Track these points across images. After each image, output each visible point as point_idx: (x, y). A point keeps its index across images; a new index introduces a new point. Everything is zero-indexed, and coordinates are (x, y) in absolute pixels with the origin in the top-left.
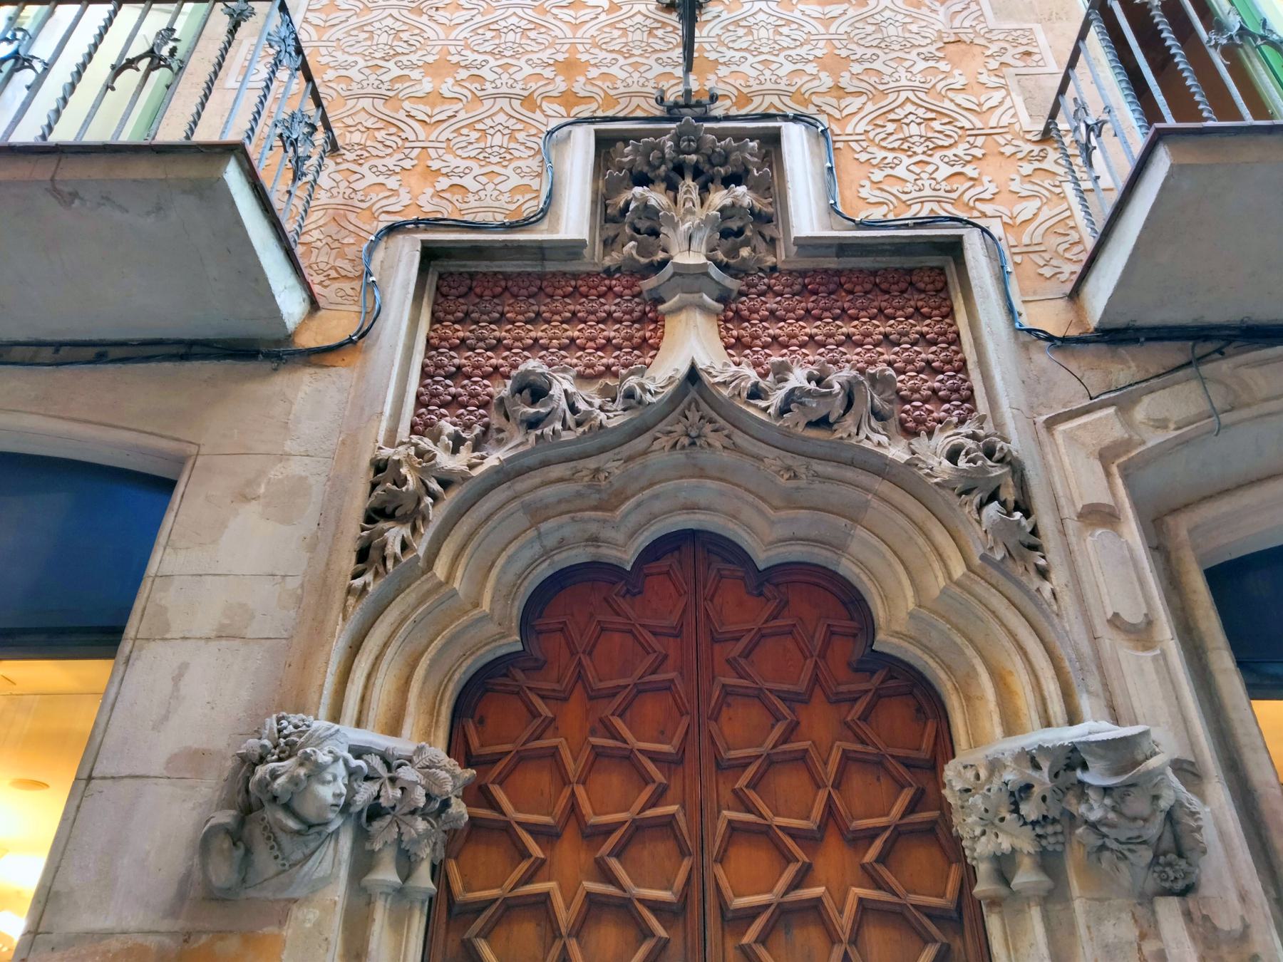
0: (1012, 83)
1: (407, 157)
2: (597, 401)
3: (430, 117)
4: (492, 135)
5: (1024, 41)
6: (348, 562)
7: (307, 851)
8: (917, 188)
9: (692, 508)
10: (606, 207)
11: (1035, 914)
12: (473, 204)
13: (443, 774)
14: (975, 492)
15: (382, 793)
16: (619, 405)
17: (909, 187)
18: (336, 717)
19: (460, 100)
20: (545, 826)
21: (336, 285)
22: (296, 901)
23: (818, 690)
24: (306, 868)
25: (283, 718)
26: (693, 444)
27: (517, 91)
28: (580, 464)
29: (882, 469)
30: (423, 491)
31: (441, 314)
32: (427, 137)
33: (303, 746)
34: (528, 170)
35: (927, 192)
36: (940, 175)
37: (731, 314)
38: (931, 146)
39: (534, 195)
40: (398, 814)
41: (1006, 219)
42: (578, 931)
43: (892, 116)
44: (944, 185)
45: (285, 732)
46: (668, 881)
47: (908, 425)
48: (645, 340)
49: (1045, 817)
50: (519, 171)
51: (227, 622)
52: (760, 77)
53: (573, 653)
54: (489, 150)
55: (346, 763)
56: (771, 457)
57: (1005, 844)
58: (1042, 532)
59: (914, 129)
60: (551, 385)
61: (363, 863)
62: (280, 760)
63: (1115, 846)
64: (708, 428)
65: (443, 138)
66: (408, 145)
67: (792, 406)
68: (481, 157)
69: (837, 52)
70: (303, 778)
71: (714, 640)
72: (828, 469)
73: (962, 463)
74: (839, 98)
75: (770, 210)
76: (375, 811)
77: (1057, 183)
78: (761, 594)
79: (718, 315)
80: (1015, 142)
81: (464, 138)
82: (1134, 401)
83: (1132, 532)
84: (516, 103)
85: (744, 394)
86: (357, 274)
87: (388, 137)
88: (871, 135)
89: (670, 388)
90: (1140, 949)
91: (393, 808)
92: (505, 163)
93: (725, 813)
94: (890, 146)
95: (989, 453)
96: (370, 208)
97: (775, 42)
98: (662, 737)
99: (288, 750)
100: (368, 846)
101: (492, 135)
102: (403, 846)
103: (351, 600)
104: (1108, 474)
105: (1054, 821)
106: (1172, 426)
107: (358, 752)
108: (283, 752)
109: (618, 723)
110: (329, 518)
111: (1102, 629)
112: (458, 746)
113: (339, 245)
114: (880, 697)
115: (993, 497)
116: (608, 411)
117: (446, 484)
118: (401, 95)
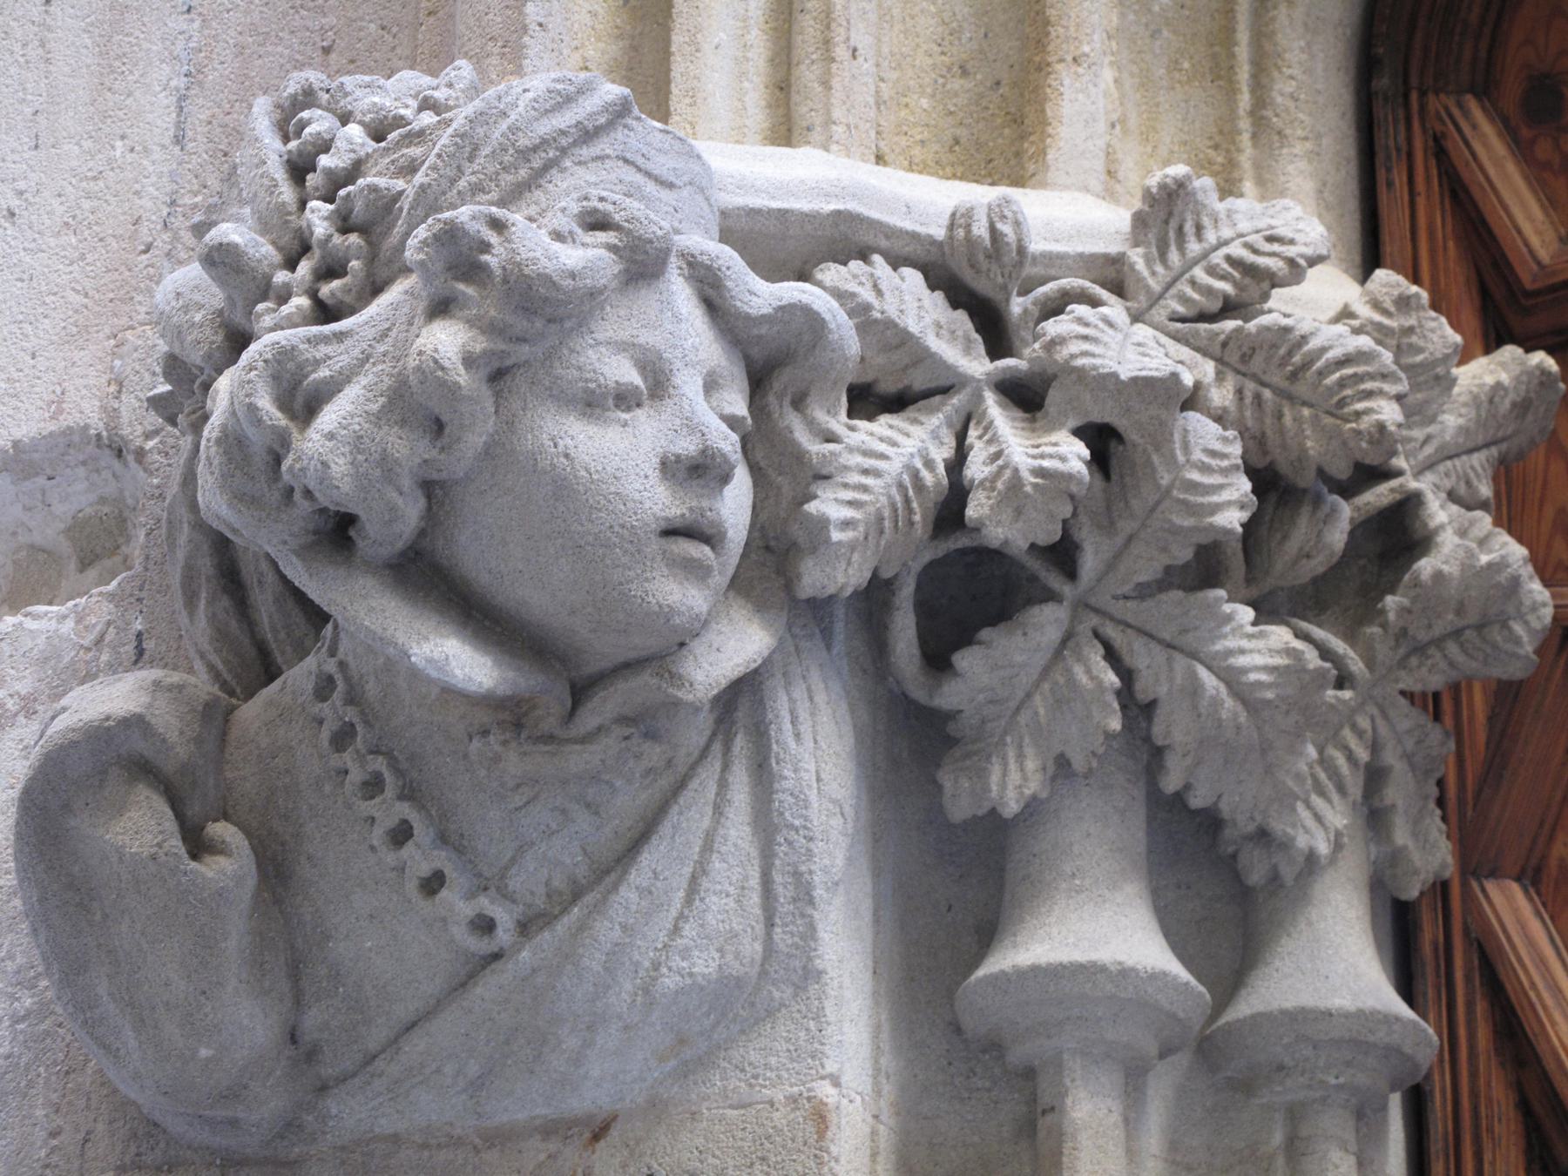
15: (977, 468)
24: (607, 931)
25: (307, 98)
40: (1103, 600)
70: (462, 377)
91: (1063, 554)
100: (960, 804)
102: (1171, 783)
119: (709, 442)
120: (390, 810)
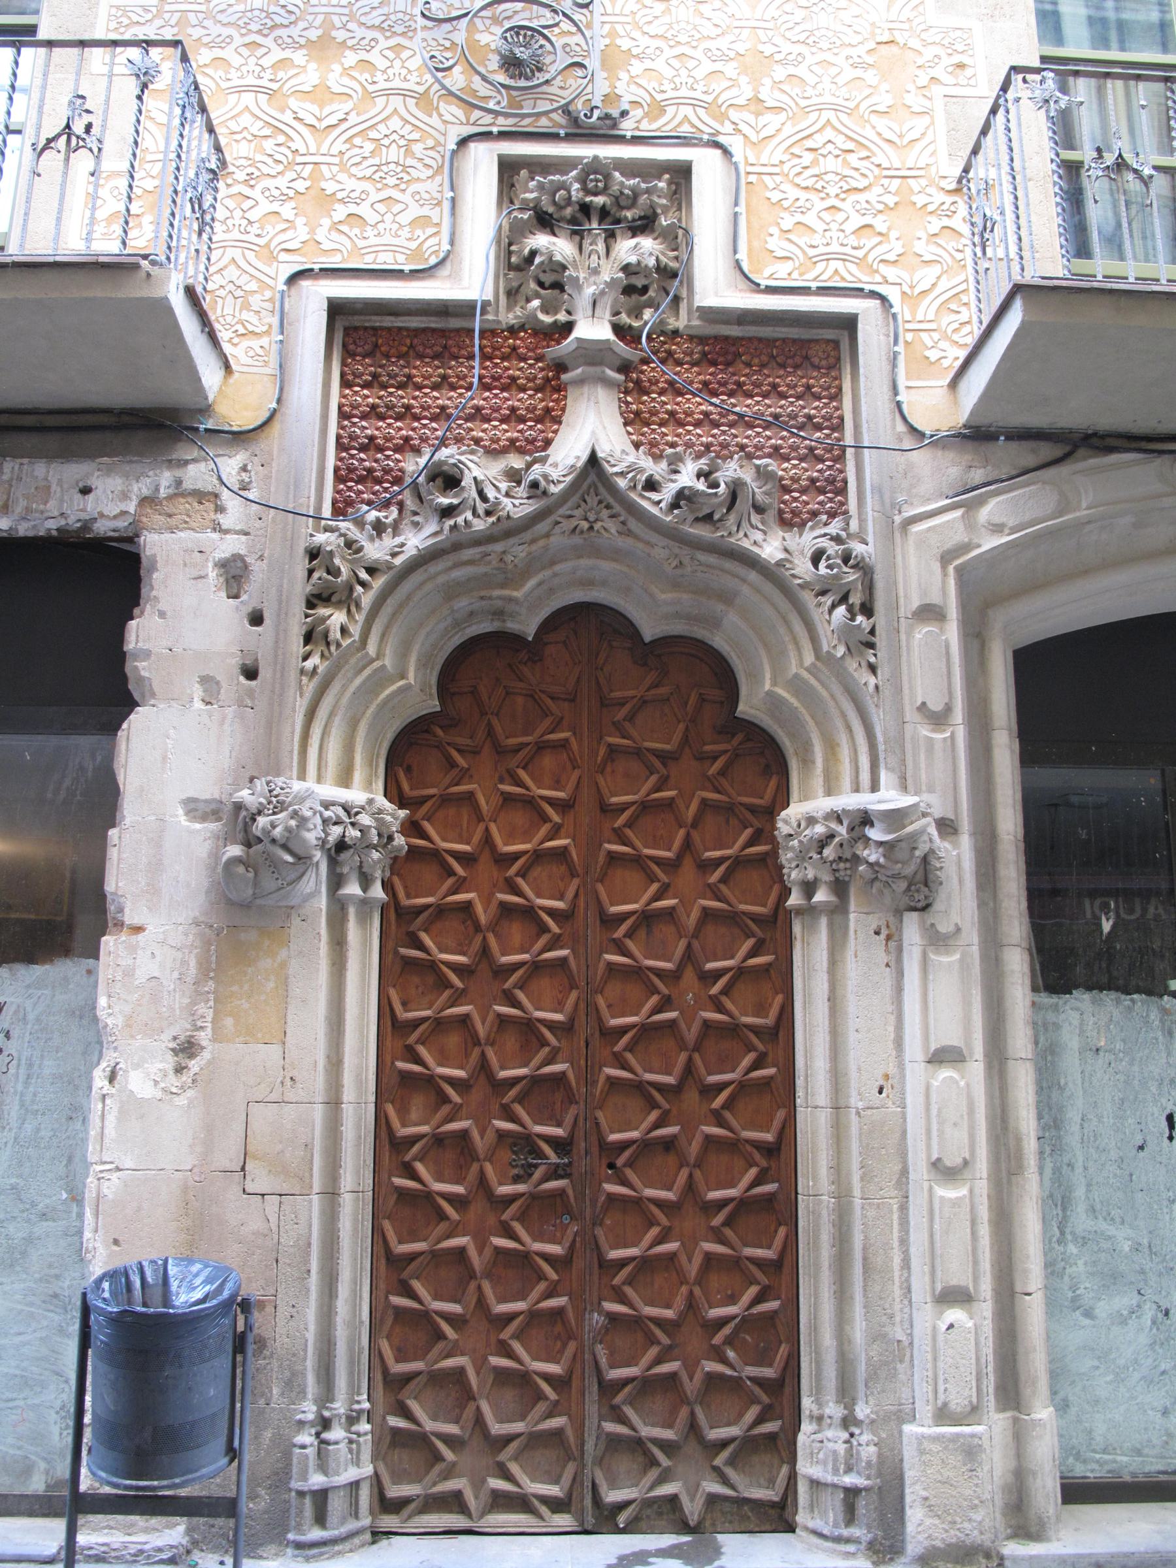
0: (939, 105)
1: (299, 177)
2: (504, 486)
3: (319, 120)
4: (387, 147)
5: (960, 48)
6: (296, 645)
9: (589, 583)
10: (510, 253)
11: (824, 921)
12: (373, 241)
13: (389, 818)
14: (830, 594)
16: (522, 491)
17: (817, 239)
18: (302, 776)
19: (350, 96)
20: (465, 853)
21: (246, 343)
23: (687, 750)
26: (591, 528)
27: (410, 85)
28: (489, 548)
29: (752, 562)
30: (354, 581)
31: (350, 378)
32: (318, 150)
33: (290, 805)
34: (427, 196)
35: (835, 247)
36: (850, 227)
38: (846, 187)
39: (435, 230)
41: (906, 289)
42: (494, 926)
43: (810, 144)
44: (853, 241)
45: (275, 793)
46: (559, 1004)
48: (548, 410)
49: (840, 858)
50: (417, 197)
52: (675, 79)
53: (483, 714)
56: (660, 544)
57: (810, 874)
58: (877, 633)
59: (831, 164)
60: (462, 472)
61: (336, 881)
62: (274, 813)
63: (884, 879)
64: (605, 513)
65: (334, 151)
66: (299, 159)
67: (682, 503)
69: (761, 47)
71: (602, 704)
72: (712, 559)
73: (823, 569)
74: (758, 114)
75: (673, 265)
76: (342, 845)
77: (961, 248)
78: (645, 664)
79: (619, 386)
81: (356, 151)
82: (981, 501)
83: (952, 632)
84: (411, 102)
85: (639, 487)
86: (265, 329)
87: (277, 148)
88: (786, 167)
89: (568, 479)
92: (403, 186)
93: (607, 846)
94: (804, 184)
95: (846, 558)
96: (268, 245)
97: (695, 28)
98: (557, 785)
99: (281, 807)
100: (338, 870)
101: (387, 147)
103: (305, 679)
104: (945, 575)
105: (847, 860)
106: (1007, 531)
107: (327, 805)
108: (275, 807)
109: (522, 773)
111: (910, 714)
112: (394, 792)
113: (242, 294)
114: (737, 755)
115: (844, 599)
116: (513, 497)
117: (371, 571)
118: (285, 88)
119: (144, 519)
120: (272, 869)
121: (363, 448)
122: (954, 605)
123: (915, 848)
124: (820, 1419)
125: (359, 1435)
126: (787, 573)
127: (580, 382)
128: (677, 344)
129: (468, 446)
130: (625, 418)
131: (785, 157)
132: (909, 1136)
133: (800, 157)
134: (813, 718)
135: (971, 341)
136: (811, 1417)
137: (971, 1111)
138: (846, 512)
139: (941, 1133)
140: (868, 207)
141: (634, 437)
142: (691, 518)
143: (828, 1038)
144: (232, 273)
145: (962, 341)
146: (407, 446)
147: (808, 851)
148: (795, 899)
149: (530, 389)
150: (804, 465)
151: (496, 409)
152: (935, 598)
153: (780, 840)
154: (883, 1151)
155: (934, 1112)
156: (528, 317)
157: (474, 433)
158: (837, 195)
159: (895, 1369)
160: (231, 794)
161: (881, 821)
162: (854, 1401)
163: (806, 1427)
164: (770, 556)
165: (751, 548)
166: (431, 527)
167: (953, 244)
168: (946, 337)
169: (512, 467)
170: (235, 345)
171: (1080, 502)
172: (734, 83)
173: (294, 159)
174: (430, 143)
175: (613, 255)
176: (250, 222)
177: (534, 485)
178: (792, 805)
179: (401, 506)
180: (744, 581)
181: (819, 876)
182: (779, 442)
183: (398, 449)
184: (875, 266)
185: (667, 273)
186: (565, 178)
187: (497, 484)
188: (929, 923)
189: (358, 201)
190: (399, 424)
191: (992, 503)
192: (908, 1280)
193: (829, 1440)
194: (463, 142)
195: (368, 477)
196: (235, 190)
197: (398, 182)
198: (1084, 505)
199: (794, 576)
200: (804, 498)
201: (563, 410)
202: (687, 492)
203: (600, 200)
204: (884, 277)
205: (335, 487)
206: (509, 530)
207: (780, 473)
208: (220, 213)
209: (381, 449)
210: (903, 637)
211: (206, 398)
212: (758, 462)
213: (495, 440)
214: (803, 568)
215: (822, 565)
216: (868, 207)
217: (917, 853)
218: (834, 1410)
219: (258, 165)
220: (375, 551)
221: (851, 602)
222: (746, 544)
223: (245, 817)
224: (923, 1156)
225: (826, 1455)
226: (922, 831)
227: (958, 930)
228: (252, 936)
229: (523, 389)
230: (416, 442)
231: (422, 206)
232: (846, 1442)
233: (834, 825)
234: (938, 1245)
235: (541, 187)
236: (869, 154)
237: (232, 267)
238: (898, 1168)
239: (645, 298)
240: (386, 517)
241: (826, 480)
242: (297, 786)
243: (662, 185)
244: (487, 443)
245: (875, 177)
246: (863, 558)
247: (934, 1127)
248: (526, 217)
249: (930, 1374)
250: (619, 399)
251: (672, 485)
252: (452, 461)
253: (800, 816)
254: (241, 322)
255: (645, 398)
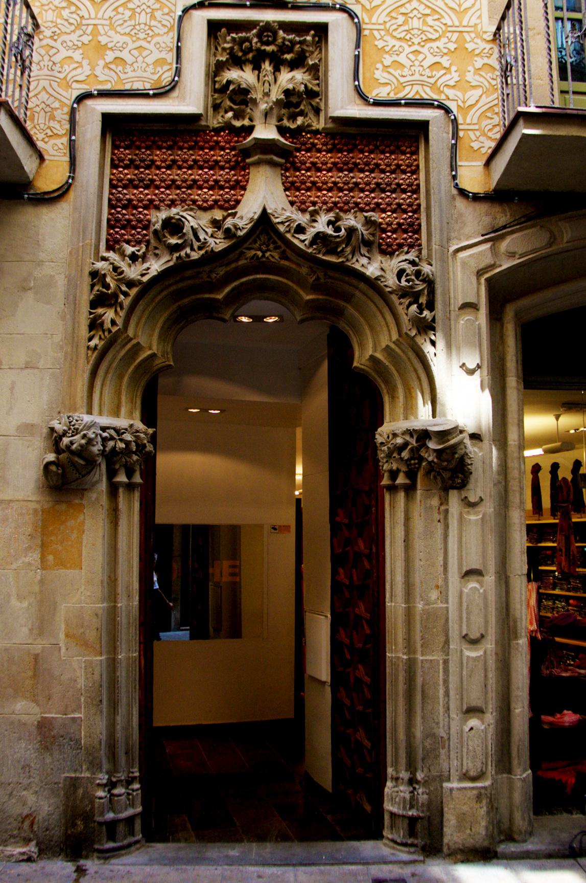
2: (210, 231)
4: (139, 14)
6: (84, 331)
7: (88, 471)
8: (411, 73)
12: (131, 74)
13: (142, 435)
16: (220, 234)
17: (406, 72)
21: (53, 141)
22: (86, 490)
29: (362, 277)
31: (117, 162)
32: (96, 15)
33: (82, 430)
35: (417, 77)
36: (426, 64)
37: (289, 165)
38: (424, 38)
41: (460, 103)
43: (403, 10)
44: (428, 72)
45: (73, 423)
47: (383, 247)
51: (29, 360)
54: (137, 27)
55: (101, 435)
61: (111, 473)
62: (72, 436)
64: (271, 246)
65: (106, 16)
68: (132, 33)
75: (316, 89)
77: (495, 77)
80: (476, 40)
81: (120, 16)
82: (502, 237)
88: (388, 25)
89: (249, 226)
90: (439, 509)
92: (149, 39)
94: (398, 36)
96: (65, 78)
99: (76, 431)
103: (90, 352)
104: (479, 283)
106: (517, 256)
107: (104, 429)
108: (73, 432)
110: (71, 300)
113: (50, 109)
115: (416, 301)
116: (215, 238)
121: (124, 207)
122: (484, 303)
123: (456, 453)
124: (397, 779)
125: (133, 790)
126: (382, 284)
127: (258, 163)
128: (318, 139)
129: (189, 205)
130: (285, 186)
131: (387, 19)
132: (450, 621)
133: (396, 19)
134: (398, 371)
135: (498, 136)
136: (392, 778)
137: (486, 606)
138: (420, 245)
139: (468, 619)
140: (438, 51)
141: (290, 198)
142: (324, 250)
143: (403, 564)
144: (44, 96)
145: (493, 137)
146: (151, 205)
147: (393, 453)
148: (385, 481)
149: (227, 168)
150: (394, 215)
151: (207, 181)
152: (472, 299)
153: (378, 445)
154: (435, 630)
155: (465, 605)
156: (225, 123)
157: (192, 197)
158: (419, 43)
159: (439, 752)
160: (48, 422)
161: (435, 437)
162: (416, 770)
163: (389, 784)
164: (372, 273)
165: (360, 269)
166: (166, 258)
167: (490, 75)
168: (484, 134)
169: (215, 219)
170: (46, 143)
171: (562, 238)
172: (80, 65)
173: (81, 22)
174: (166, 10)
175: (278, 83)
176: (54, 64)
177: (228, 230)
178: (385, 424)
179: (148, 242)
180: (357, 288)
181: (400, 467)
182: (380, 201)
183: (146, 207)
184: (441, 89)
185: (311, 94)
186: (248, 35)
187: (206, 230)
188: (463, 497)
189: (121, 49)
190: (146, 191)
191: (508, 240)
192: (448, 703)
193: (401, 791)
194: (186, 11)
195: (128, 225)
196: (45, 42)
197: (146, 36)
198: (565, 240)
199: (386, 286)
200: (394, 236)
201: (247, 181)
202: (321, 235)
203: (270, 48)
204: (447, 96)
205: (108, 231)
206: (212, 258)
207: (380, 220)
208: (36, 58)
209: (136, 207)
210: (452, 322)
211: (28, 177)
212: (366, 214)
213: (206, 201)
214: (391, 281)
215: (403, 279)
216: (438, 51)
217: (457, 456)
218: (404, 775)
219: (59, 26)
220: (132, 272)
221: (420, 302)
222: (357, 266)
223: (56, 437)
224: (457, 632)
225: (400, 800)
226: (461, 442)
227: (481, 499)
228: (63, 507)
229: (223, 168)
230: (157, 203)
231: (161, 51)
232: (411, 792)
233: (408, 438)
234: (465, 683)
235: (234, 39)
236: (439, 17)
237: (44, 93)
238: (442, 639)
239: (297, 110)
240: (138, 251)
241: (408, 224)
242: (87, 418)
243: (309, 38)
244: (200, 203)
245: (443, 31)
246: (428, 275)
247: (464, 615)
248: (224, 59)
249: (459, 755)
250: (282, 174)
251: (312, 230)
252: (177, 217)
253: (388, 432)
254: (49, 128)
255: (298, 173)
